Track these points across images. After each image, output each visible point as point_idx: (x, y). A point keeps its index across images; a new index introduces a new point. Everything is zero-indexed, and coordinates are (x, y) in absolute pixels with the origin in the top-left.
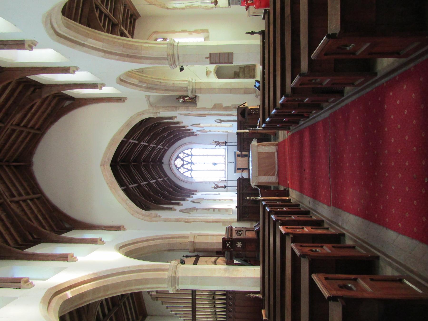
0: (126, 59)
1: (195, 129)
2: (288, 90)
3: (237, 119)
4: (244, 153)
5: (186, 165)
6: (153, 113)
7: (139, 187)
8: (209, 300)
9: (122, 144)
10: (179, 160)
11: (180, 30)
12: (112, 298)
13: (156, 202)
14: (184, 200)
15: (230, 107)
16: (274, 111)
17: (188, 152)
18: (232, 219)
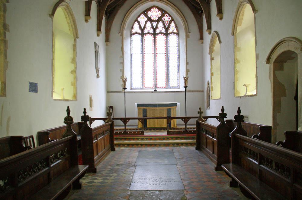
10: (159, 14)
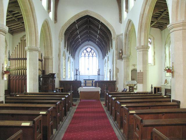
0: (140, 25)
1: (106, 58)
4: (94, 84)
6: (114, 37)
7: (76, 30)
9: (99, 21)
10: (90, 50)
12: (22, 17)
14: (70, 53)
17: (94, 54)
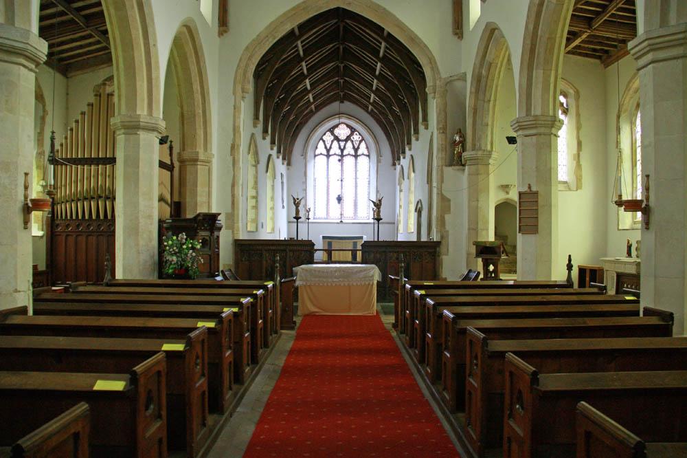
1: (405, 162)
2: (463, 324)
3: (422, 240)
5: (337, 146)
7: (298, 60)
8: (96, 189)
10: (348, 131)
11: (581, 139)
12: (101, 14)
13: (269, 90)
14: (273, 142)
15: (445, 228)
16: (432, 303)
17: (363, 149)
18: (238, 230)
